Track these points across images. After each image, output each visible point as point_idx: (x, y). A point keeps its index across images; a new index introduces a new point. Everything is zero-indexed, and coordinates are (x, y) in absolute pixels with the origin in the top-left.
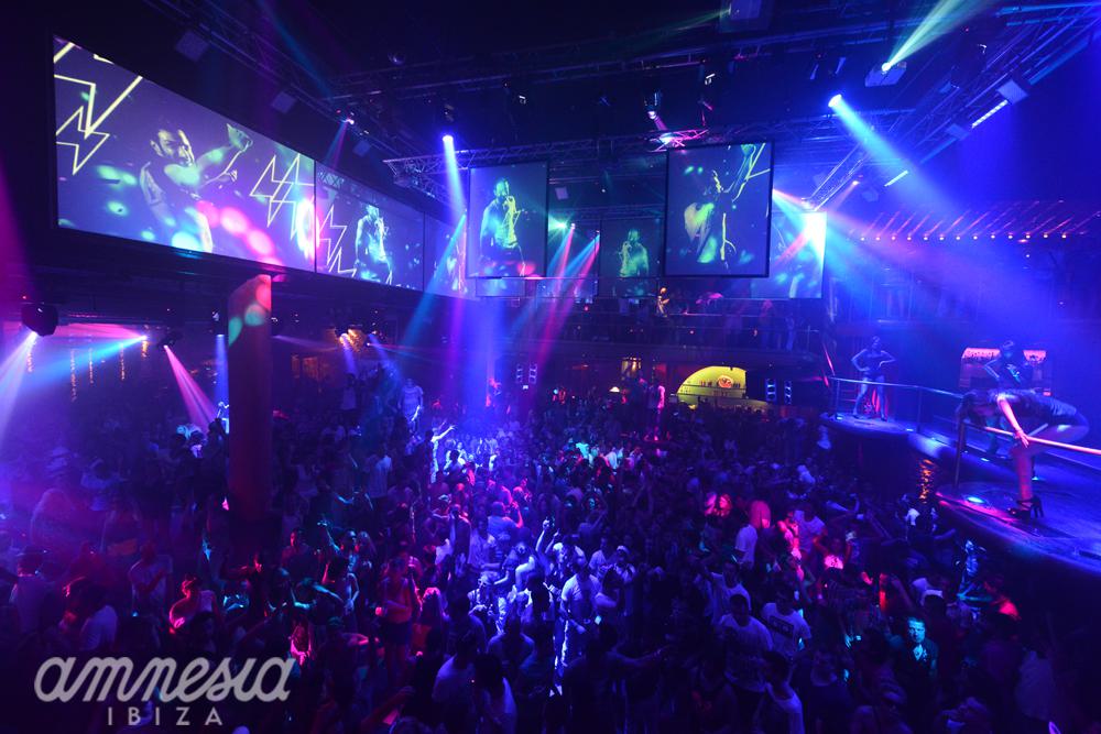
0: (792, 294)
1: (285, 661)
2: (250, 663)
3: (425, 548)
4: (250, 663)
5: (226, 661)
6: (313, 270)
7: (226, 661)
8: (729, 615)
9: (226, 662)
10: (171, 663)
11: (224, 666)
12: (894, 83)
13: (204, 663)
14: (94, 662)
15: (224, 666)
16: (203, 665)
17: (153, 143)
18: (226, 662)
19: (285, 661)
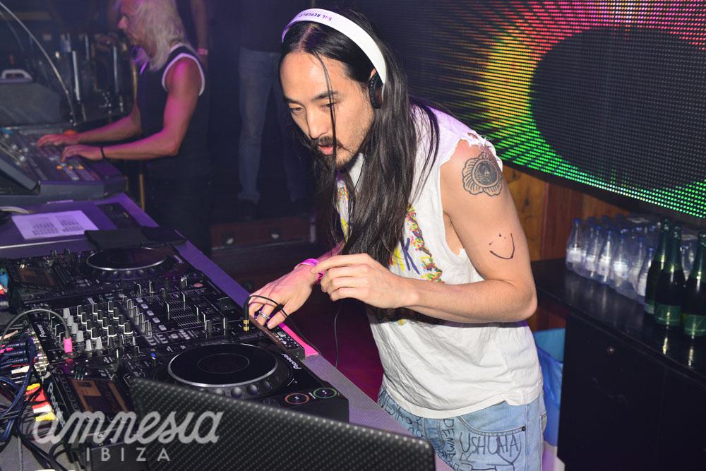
0: (46, 357)
1: (216, 414)
2: (190, 415)
3: (599, 227)
4: (190, 415)
5: (173, 414)
6: (273, 308)
7: (173, 414)
8: (126, 178)
9: (172, 415)
10: (133, 416)
11: (171, 418)
12: (449, 159)
13: (156, 415)
14: (77, 414)
15: (171, 418)
16: (155, 416)
17: (592, 229)
18: (172, 415)
19: (216, 414)
